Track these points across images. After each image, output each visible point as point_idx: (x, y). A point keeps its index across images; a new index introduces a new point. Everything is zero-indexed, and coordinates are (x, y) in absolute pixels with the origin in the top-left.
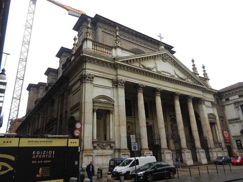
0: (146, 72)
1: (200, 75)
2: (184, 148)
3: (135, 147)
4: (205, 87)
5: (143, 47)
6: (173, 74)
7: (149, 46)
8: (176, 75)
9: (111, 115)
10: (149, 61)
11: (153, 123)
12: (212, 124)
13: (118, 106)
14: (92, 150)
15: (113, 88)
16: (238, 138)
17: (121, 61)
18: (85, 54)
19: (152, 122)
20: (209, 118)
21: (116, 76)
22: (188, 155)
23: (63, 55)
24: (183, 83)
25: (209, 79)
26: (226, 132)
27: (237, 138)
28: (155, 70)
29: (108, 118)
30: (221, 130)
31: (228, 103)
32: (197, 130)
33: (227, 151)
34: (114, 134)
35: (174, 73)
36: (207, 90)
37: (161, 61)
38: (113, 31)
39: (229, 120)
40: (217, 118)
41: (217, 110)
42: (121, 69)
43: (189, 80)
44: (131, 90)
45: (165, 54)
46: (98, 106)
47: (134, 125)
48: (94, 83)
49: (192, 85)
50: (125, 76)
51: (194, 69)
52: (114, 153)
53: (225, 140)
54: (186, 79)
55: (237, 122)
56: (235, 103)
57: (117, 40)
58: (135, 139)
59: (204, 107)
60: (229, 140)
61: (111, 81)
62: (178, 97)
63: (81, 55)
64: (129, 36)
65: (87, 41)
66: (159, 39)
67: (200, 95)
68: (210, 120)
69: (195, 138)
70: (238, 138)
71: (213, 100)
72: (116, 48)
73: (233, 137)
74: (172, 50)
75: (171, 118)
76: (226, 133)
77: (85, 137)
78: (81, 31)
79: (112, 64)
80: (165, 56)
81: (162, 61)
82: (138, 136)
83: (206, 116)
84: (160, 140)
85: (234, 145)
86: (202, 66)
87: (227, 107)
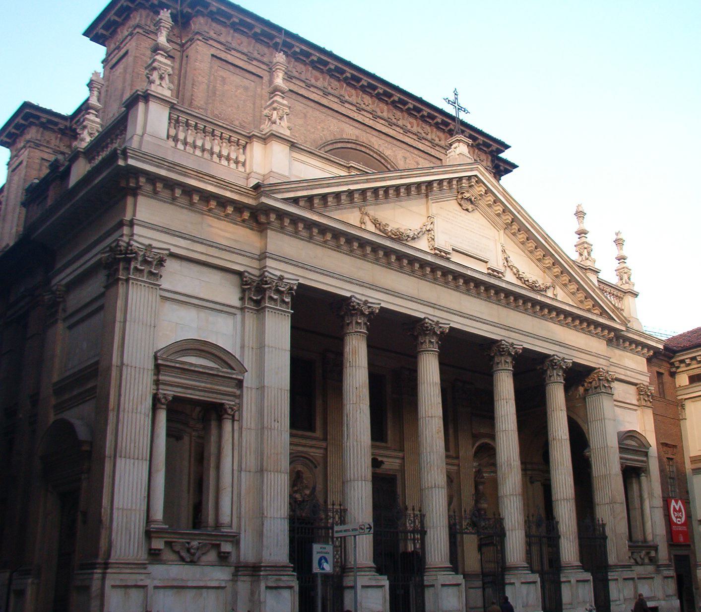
1: (601, 276)
2: (516, 568)
4: (618, 326)
5: (383, 137)
6: (497, 263)
7: (406, 131)
9: (227, 426)
10: (403, 203)
11: (403, 466)
12: (632, 474)
13: (261, 388)
14: (143, 566)
15: (242, 309)
17: (286, 200)
19: (397, 461)
20: (623, 449)
21: (260, 260)
22: (528, 594)
23: (28, 137)
24: (535, 303)
28: (423, 244)
29: (213, 438)
30: (663, 497)
33: (672, 577)
34: (236, 502)
35: (501, 257)
36: (626, 339)
37: (452, 205)
42: (282, 229)
47: (320, 468)
48: (165, 283)
51: (584, 247)
52: (232, 580)
54: (548, 288)
57: (275, 105)
61: (235, 279)
62: (509, 360)
63: (121, 163)
66: (450, 110)
68: (627, 459)
71: (645, 380)
75: (475, 447)
77: (115, 511)
78: (118, 48)
81: (459, 208)
82: (337, 517)
83: (613, 442)
84: (423, 533)
86: (615, 237)
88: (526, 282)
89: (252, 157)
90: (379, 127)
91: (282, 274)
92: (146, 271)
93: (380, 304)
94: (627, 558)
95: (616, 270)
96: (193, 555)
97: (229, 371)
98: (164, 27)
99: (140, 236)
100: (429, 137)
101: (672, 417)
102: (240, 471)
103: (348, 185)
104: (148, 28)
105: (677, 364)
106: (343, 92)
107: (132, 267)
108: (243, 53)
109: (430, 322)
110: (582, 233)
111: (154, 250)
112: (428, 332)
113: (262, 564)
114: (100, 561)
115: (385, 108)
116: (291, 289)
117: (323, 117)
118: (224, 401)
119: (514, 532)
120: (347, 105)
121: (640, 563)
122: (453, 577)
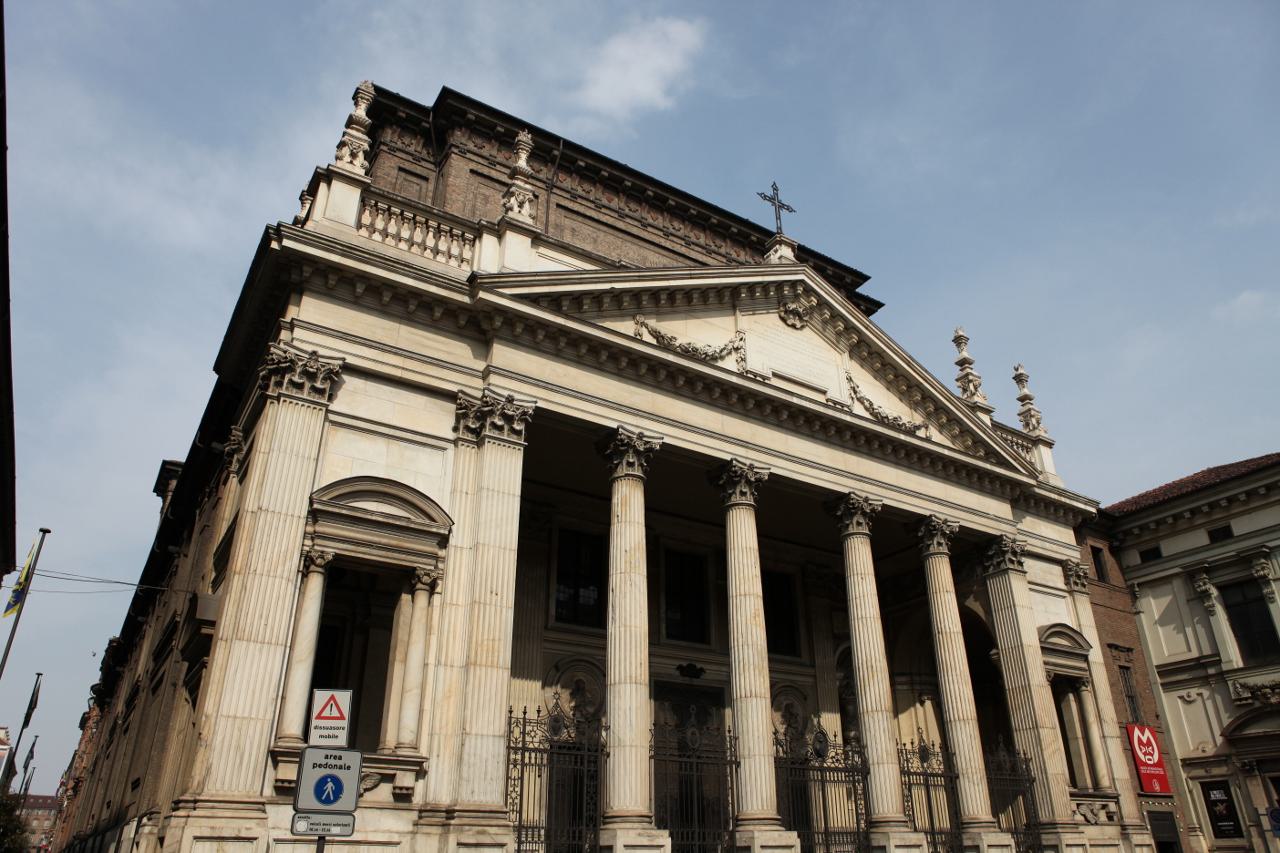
3: (330, 785)
6: (839, 392)
12: (1065, 686)
14: (261, 805)
26: (1147, 733)
28: (730, 363)
32: (974, 714)
33: (1148, 845)
40: (1096, 655)
41: (1095, 613)
43: (936, 436)
46: (342, 541)
50: (534, 379)
58: (345, 723)
59: (1017, 584)
60: (1162, 779)
71: (1074, 555)
72: (499, 229)
73: (1188, 763)
74: (860, 290)
75: (838, 653)
76: (1144, 739)
79: (461, 306)
83: (1031, 640)
86: (1014, 373)
88: (886, 420)
90: (693, 255)
91: (512, 393)
93: (536, 402)
94: (1070, 812)
95: (1019, 415)
97: (428, 522)
98: (362, 98)
101: (1120, 608)
102: (438, 664)
103: (611, 282)
104: (393, 144)
105: (1121, 536)
106: (645, 215)
107: (286, 380)
109: (740, 465)
110: (963, 363)
111: (320, 359)
112: (737, 479)
113: (456, 808)
115: (702, 235)
116: (524, 413)
117: (619, 242)
118: (415, 565)
119: (881, 766)
121: (1093, 822)
122: (780, 836)
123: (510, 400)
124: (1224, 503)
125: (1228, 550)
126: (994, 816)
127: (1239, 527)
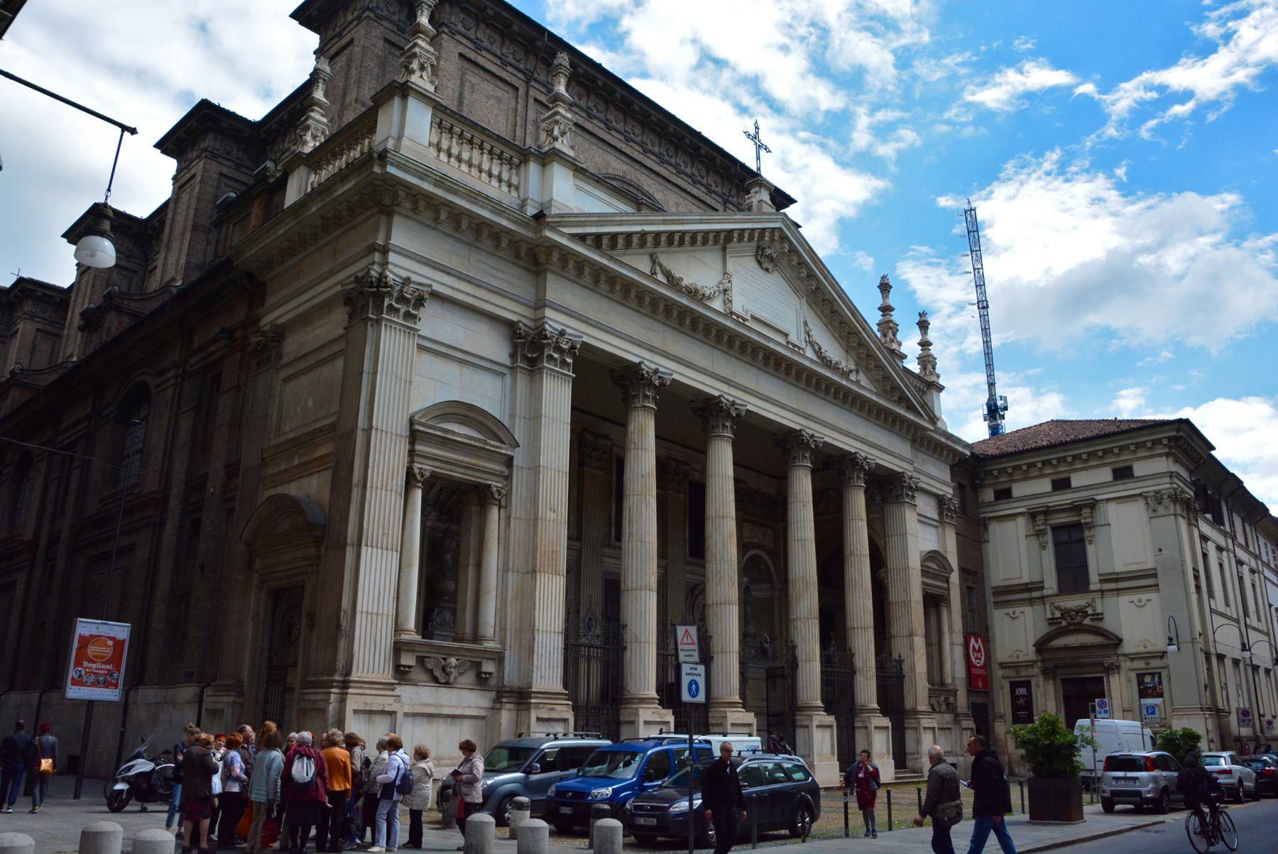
0: (684, 312)
4: (926, 425)
8: (812, 344)
9: (494, 513)
12: (934, 602)
15: (512, 369)
16: (1023, 672)
18: (399, 166)
20: (925, 572)
21: (535, 309)
25: (941, 389)
27: (1018, 672)
28: (717, 304)
31: (1006, 508)
37: (751, 263)
38: (514, 62)
39: (999, 591)
44: (606, 391)
45: (773, 229)
49: (876, 404)
50: (577, 317)
51: (888, 327)
53: (971, 678)
54: (851, 371)
55: (1031, 601)
56: (1032, 515)
57: (558, 117)
58: (696, 647)
59: (910, 516)
63: (377, 169)
64: (590, 105)
65: (404, 97)
67: (901, 458)
69: (858, 663)
70: (1023, 672)
73: (1003, 666)
78: (340, 36)
80: (772, 240)
83: (915, 563)
85: (1003, 702)
87: (995, 528)
89: (526, 178)
90: (649, 164)
92: (402, 311)
96: (448, 674)
99: (396, 265)
100: (704, 181)
108: (496, 56)
114: (337, 678)
120: (613, 133)
123: (562, 333)
124: (1069, 459)
125: (1065, 498)
126: (565, 686)
127: (1077, 480)
